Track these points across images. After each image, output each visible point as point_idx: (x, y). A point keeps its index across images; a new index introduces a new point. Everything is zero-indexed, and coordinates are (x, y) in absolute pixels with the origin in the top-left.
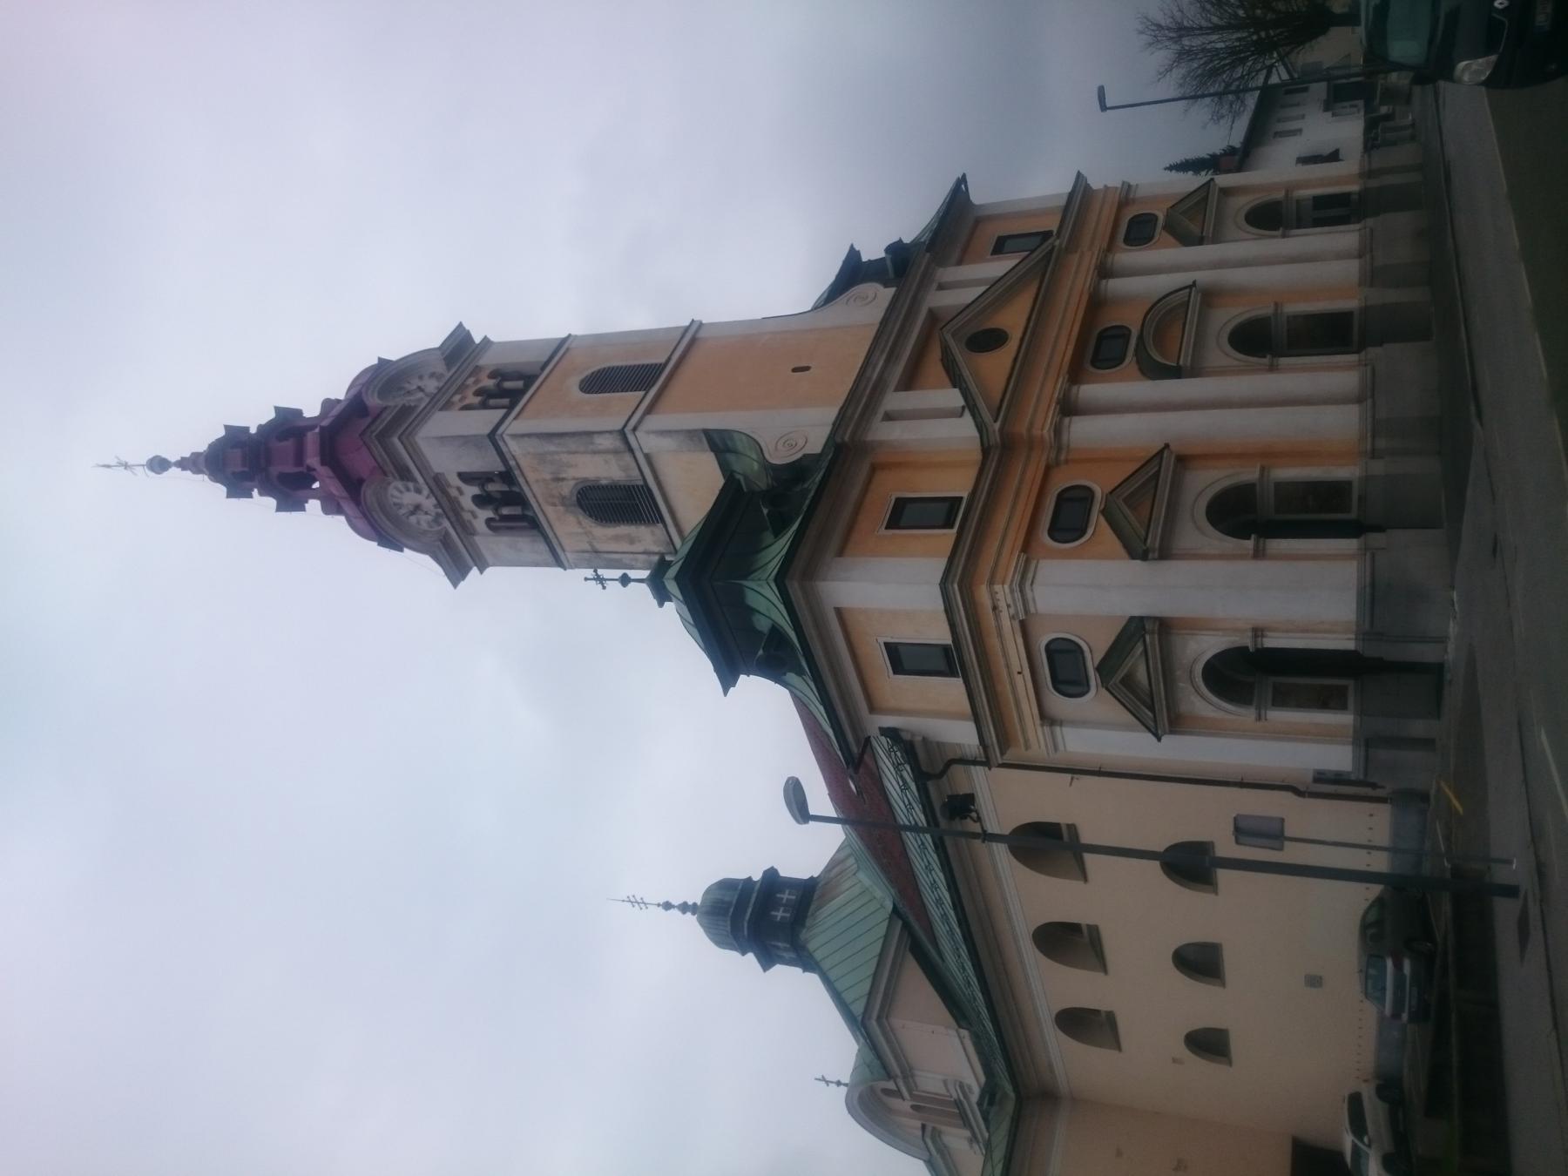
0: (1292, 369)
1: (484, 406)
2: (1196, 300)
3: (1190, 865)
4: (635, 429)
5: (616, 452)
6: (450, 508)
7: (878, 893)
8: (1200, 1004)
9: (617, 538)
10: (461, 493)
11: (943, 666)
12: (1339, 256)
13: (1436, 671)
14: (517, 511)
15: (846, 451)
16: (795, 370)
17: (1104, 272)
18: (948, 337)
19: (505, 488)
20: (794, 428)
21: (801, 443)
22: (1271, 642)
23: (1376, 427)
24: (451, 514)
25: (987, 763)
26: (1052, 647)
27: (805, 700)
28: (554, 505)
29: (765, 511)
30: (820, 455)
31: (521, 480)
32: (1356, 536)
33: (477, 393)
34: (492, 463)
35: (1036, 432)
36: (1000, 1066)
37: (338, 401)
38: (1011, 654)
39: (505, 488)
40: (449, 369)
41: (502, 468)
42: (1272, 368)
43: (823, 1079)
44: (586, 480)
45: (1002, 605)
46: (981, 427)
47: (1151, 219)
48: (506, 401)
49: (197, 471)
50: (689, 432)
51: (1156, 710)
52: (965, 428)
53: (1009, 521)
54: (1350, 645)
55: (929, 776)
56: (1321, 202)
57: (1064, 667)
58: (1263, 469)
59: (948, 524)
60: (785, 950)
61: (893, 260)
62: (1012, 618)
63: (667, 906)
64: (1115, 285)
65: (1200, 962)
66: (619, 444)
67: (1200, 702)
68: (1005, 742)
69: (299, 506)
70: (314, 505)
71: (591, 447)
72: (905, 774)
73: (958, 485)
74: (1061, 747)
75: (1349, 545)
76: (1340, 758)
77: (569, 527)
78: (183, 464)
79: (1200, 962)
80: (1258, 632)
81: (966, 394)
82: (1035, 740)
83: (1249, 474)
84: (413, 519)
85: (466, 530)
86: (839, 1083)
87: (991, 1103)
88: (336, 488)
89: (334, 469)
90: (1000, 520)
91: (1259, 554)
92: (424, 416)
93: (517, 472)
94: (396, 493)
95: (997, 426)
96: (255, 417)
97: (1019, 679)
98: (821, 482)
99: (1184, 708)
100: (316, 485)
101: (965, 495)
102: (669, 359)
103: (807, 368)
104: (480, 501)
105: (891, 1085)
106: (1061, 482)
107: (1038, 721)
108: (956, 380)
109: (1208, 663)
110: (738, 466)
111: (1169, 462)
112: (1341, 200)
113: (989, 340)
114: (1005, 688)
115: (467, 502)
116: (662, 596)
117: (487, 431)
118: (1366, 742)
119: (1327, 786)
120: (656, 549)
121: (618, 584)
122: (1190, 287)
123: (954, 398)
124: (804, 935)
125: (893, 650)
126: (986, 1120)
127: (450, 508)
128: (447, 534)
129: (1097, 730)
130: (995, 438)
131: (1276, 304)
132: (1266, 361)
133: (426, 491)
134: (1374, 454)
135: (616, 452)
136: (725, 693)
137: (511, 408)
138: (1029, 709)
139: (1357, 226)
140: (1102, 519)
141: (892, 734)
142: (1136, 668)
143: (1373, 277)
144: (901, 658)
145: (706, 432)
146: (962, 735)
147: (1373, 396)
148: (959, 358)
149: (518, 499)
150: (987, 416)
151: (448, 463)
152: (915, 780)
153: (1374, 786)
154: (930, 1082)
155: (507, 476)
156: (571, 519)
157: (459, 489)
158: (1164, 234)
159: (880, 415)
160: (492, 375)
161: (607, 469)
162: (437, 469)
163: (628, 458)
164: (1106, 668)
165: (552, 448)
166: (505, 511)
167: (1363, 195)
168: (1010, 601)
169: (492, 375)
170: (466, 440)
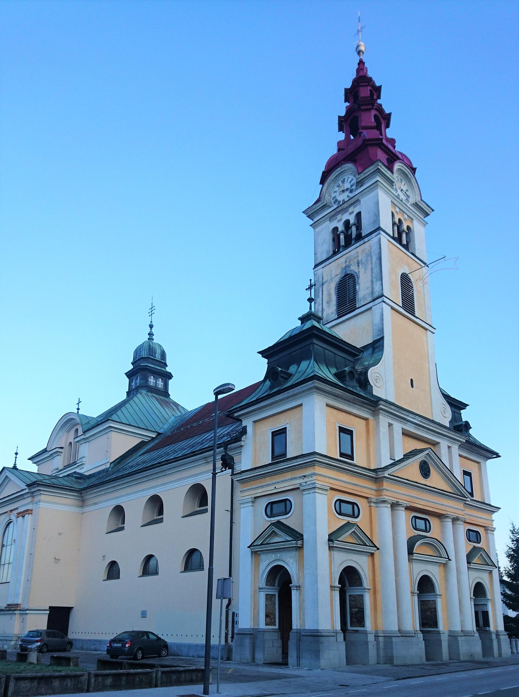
0: (412, 602)
1: (394, 224)
2: (443, 561)
3: (192, 560)
4: (384, 302)
5: (372, 293)
6: (342, 207)
7: (166, 426)
8: (131, 567)
9: (329, 295)
10: (350, 214)
11: (276, 454)
12: (462, 622)
13: (284, 663)
14: (342, 243)
15: (374, 404)
16: (412, 380)
17: (455, 520)
18: (427, 452)
19: (354, 236)
20: (384, 380)
21: (378, 385)
22: (294, 594)
23: (388, 637)
24: (340, 208)
25: (233, 474)
26: (288, 502)
27: (258, 390)
28: (346, 262)
29: (346, 369)
30: (372, 394)
31: (357, 244)
32: (342, 629)
33: (400, 220)
34: (366, 229)
35: (385, 492)
36: (93, 481)
37: (394, 147)
38: (283, 483)
39: (354, 236)
40: (411, 205)
41: (363, 235)
42: (412, 593)
43: (80, 402)
44: (358, 278)
45: (306, 480)
46: (386, 468)
47: (478, 541)
48: (396, 235)
49: (358, 71)
50: (383, 329)
51: (257, 549)
52: (386, 462)
53: (344, 480)
54: (294, 627)
55: (226, 449)
56: (486, 614)
57: (278, 507)
58: (369, 589)
59: (342, 455)
60: (136, 383)
61: (461, 425)
62: (300, 484)
63: (151, 326)
64: (449, 524)
65: (149, 567)
66: (376, 295)
67: (267, 562)
68: (242, 481)
69: (341, 129)
70: (342, 136)
71: (375, 280)
72: (226, 438)
73: (359, 459)
74: (242, 506)
75: (338, 627)
76: (245, 623)
77: (333, 272)
78: (361, 63)
79: (149, 567)
80: (298, 587)
81: (401, 461)
82: (244, 494)
83: (367, 583)
84: (280, 379)
85: (332, 217)
86: (78, 409)
87: (76, 478)
88: (351, 149)
89: (360, 147)
90: (344, 477)
91: (332, 587)
92: (388, 193)
93: (362, 242)
94: (350, 180)
95: (386, 475)
96: (386, 102)
97: (272, 487)
98: (361, 395)
99: (263, 557)
100: (352, 137)
101: (355, 462)
102: (417, 318)
103: (412, 386)
104: (347, 223)
105: (80, 432)
106: (362, 503)
107: (253, 496)
108: (407, 456)
109: (282, 567)
110: (366, 354)
111: (372, 550)
112: (487, 623)
113: (425, 470)
114: (268, 480)
115: (346, 217)
116: (304, 319)
117: (382, 226)
118: (253, 634)
119: (231, 619)
120: (324, 315)
121: (309, 297)
122: (448, 558)
123: (399, 456)
124: (144, 392)
125: (283, 431)
126: (68, 475)
127: (342, 207)
128: (330, 207)
129: (252, 521)
130: (380, 474)
131: (440, 595)
132: (416, 591)
133: (351, 195)
134: (376, 636)
135: (372, 293)
136: (259, 353)
137: (393, 238)
138: (259, 492)
139: (475, 630)
140: (346, 522)
141: (244, 431)
142: (283, 532)
143: (453, 636)
144: (279, 434)
145: (382, 338)
146: (245, 461)
147: (401, 636)
148: (417, 457)
149: (348, 243)
150: (390, 471)
151: (364, 206)
152: (223, 442)
153: (232, 637)
154: (84, 450)
155: (359, 237)
156: (339, 271)
157: (352, 212)
158: (472, 547)
159: (391, 422)
160: (408, 228)
161: (363, 290)
162: (362, 201)
163: (370, 299)
164: (279, 525)
165: (374, 260)
166: (342, 237)
167: (489, 633)
168: (308, 483)
169: (408, 228)
170: (377, 215)
